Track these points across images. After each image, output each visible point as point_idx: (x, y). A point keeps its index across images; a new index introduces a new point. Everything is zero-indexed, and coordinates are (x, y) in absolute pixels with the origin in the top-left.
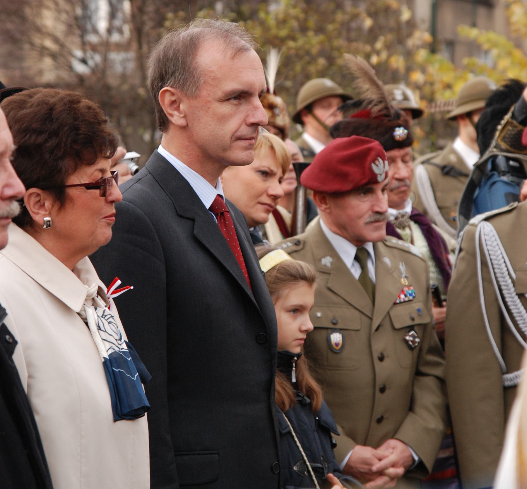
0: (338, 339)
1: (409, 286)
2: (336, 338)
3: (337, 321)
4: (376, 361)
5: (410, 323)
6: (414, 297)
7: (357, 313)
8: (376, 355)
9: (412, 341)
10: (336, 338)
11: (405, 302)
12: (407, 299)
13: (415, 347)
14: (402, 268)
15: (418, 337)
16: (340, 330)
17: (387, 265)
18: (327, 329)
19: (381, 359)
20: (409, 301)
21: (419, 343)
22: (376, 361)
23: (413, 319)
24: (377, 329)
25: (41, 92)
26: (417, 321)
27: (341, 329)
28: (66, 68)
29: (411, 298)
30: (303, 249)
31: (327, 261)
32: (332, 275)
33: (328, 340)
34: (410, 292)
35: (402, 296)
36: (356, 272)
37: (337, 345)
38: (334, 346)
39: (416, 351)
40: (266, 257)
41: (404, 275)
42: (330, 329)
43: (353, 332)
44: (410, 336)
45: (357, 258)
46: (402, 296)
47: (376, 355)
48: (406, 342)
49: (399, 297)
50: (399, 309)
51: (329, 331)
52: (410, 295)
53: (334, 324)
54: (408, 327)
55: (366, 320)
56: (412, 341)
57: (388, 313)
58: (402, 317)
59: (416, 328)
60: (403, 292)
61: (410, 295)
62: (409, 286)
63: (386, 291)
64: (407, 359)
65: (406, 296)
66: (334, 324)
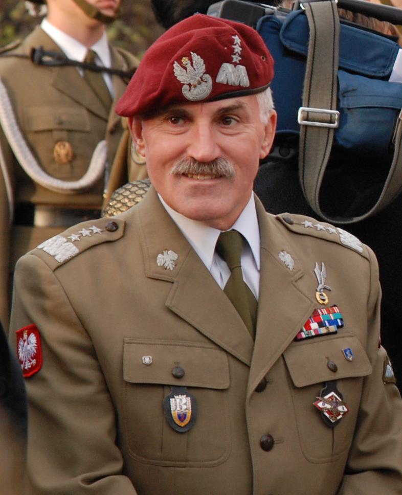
0: (184, 407)
1: (330, 308)
2: (181, 404)
3: (183, 371)
4: (256, 449)
5: (327, 376)
6: (338, 327)
7: (224, 356)
8: (255, 439)
9: (329, 412)
10: (181, 404)
11: (318, 335)
12: (323, 331)
13: (338, 422)
14: (320, 273)
15: (343, 403)
16: (186, 390)
17: (287, 266)
18: (163, 386)
19: (267, 446)
20: (329, 334)
21: (345, 413)
22: (256, 449)
23: (334, 370)
24: (261, 388)
25: (161, 41)
26: (342, 373)
27: (189, 388)
28: (187, 172)
29: (333, 328)
30: (122, 237)
31: (167, 259)
32: (175, 285)
33: (166, 408)
34: (332, 317)
35: (314, 325)
36: (220, 275)
37: (182, 417)
38: (177, 422)
39: (343, 432)
40: (124, 357)
41: (320, 286)
42: (169, 386)
43: (212, 393)
44: (326, 401)
45: (221, 251)
46: (314, 325)
47: (255, 439)
48: (319, 412)
49: (308, 327)
50: (305, 349)
51: (167, 392)
52: (331, 322)
53: (178, 377)
54: (323, 384)
55: (238, 369)
56: (329, 412)
57: (282, 355)
58: (309, 366)
59: (340, 386)
60: (315, 315)
61: (331, 322)
62: (330, 308)
63: (281, 317)
64: (320, 445)
65: (321, 325)
66: (178, 377)
